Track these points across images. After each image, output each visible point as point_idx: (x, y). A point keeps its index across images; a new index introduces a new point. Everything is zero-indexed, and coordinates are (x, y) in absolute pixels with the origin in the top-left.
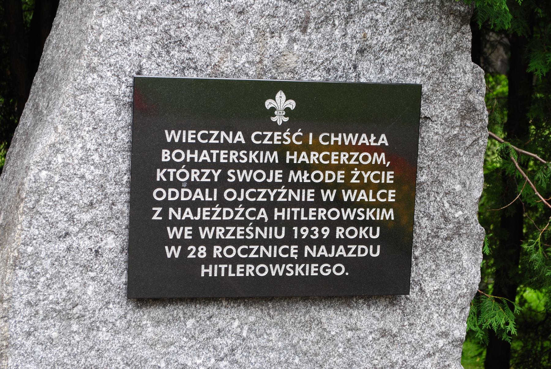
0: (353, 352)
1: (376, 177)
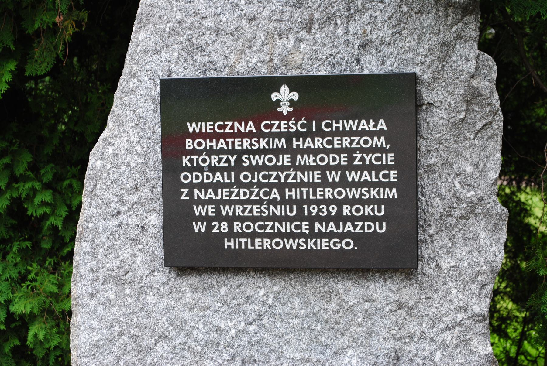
0: (372, 322)
1: (378, 159)
